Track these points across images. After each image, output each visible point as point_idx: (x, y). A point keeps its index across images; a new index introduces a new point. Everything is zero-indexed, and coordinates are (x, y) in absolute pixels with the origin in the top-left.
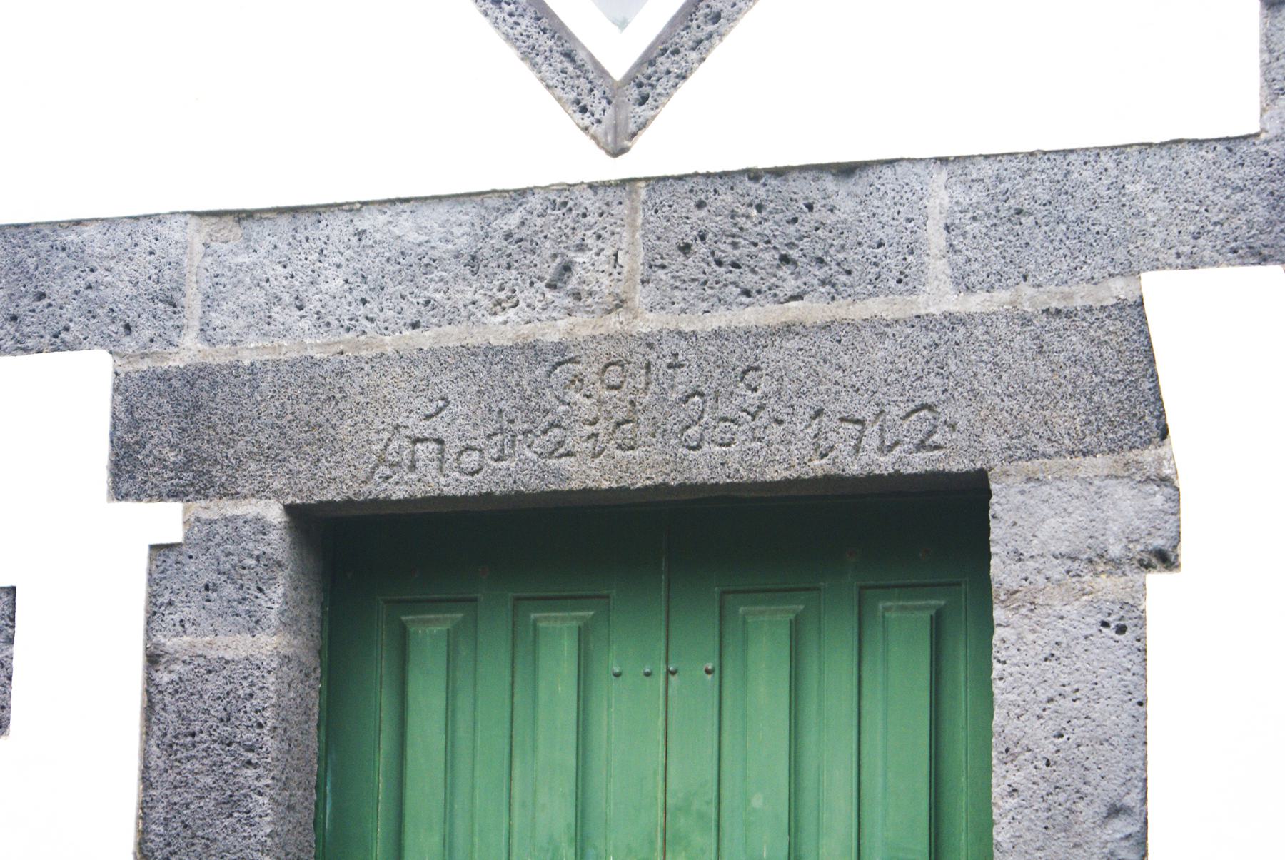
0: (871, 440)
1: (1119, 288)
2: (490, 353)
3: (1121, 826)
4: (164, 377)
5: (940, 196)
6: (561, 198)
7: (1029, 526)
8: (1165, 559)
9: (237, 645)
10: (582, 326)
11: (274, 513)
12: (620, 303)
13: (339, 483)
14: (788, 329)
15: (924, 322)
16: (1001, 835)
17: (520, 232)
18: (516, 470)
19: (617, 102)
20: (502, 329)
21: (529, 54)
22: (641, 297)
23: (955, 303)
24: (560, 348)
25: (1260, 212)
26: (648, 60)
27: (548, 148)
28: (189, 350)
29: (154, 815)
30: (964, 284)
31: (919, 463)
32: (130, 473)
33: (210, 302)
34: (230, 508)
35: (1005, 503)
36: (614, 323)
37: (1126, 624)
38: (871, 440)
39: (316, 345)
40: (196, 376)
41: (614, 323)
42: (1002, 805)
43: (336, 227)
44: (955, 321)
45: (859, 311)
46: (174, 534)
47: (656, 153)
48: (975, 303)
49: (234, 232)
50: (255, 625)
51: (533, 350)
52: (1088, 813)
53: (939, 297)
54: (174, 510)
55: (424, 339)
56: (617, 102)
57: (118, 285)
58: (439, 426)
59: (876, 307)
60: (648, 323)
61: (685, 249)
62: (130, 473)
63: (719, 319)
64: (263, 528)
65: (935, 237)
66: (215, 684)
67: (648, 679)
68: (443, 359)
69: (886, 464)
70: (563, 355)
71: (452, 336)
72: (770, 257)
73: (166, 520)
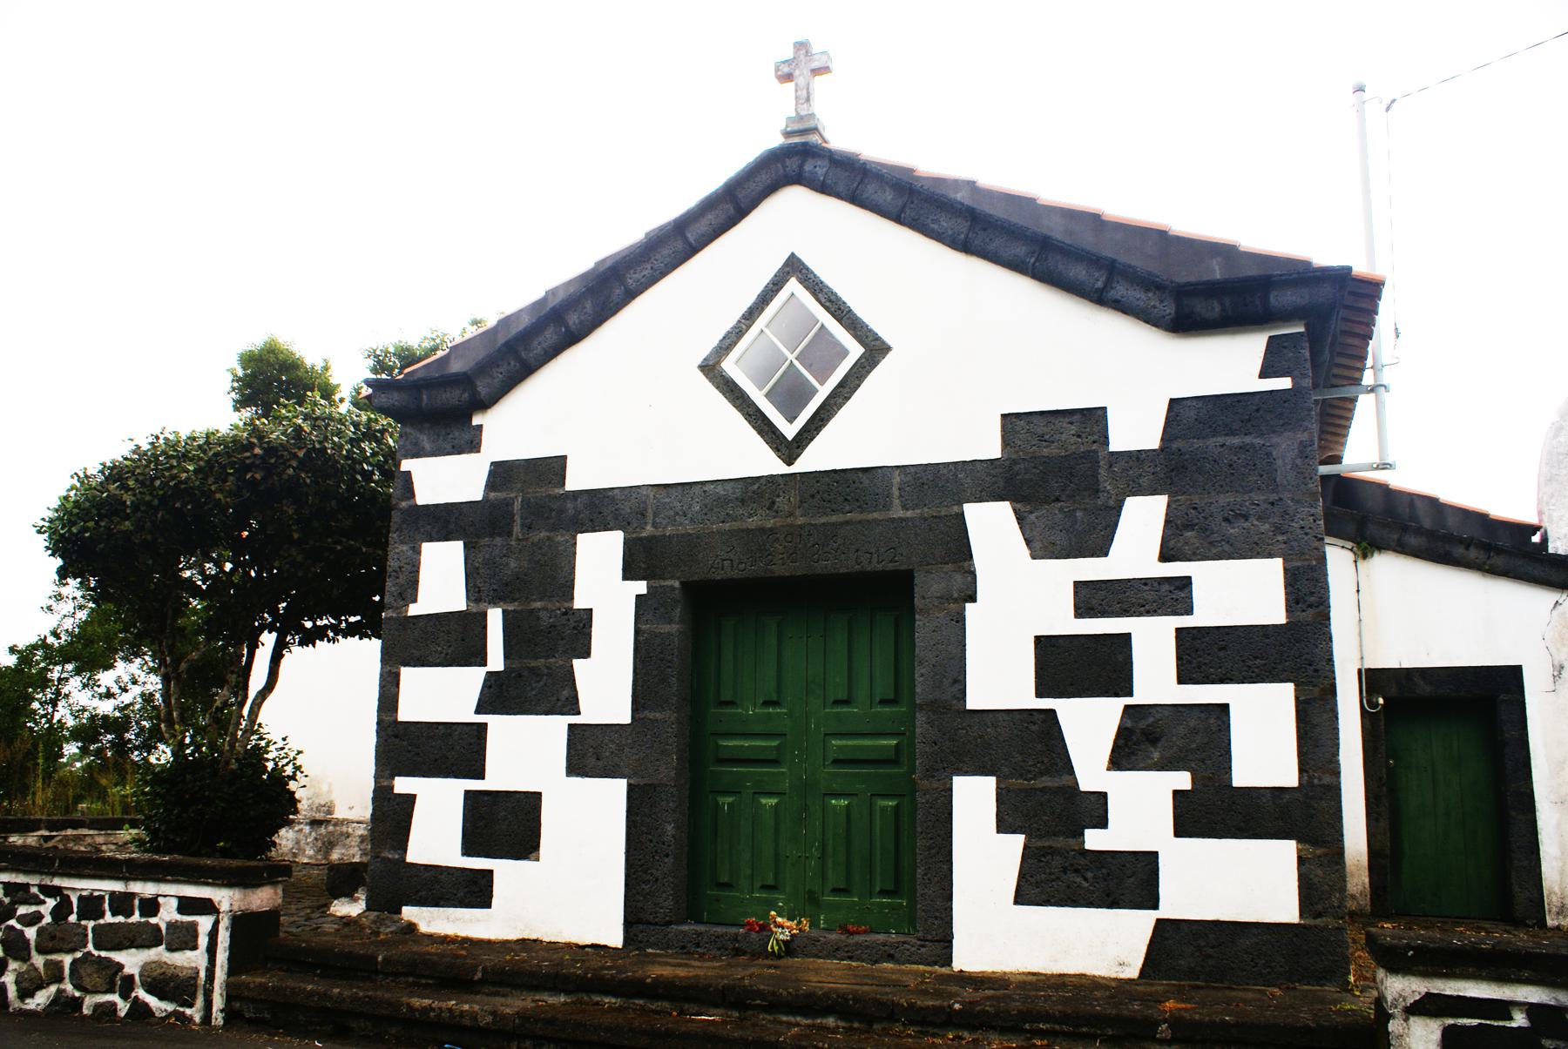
0: (875, 560)
1: (956, 509)
2: (748, 531)
3: (957, 686)
4: (641, 539)
5: (897, 479)
6: (771, 479)
7: (928, 586)
8: (973, 599)
9: (666, 628)
10: (779, 522)
11: (677, 584)
12: (791, 514)
13: (698, 574)
14: (847, 523)
15: (893, 520)
16: (918, 690)
17: (753, 490)
18: (757, 569)
19: (789, 450)
20: (752, 522)
21: (760, 433)
22: (798, 512)
23: (901, 514)
24: (771, 529)
25: (1001, 484)
26: (800, 434)
27: (767, 463)
28: (649, 530)
29: (788, 162)
30: (905, 508)
31: (891, 566)
32: (629, 573)
33: (655, 515)
34: (663, 583)
35: (919, 578)
36: (789, 520)
37: (960, 620)
38: (875, 560)
39: (690, 529)
40: (651, 538)
41: (789, 520)
42: (919, 679)
43: (697, 490)
44: (902, 519)
45: (870, 517)
46: (644, 591)
47: (808, 462)
48: (909, 514)
49: (664, 492)
50: (670, 622)
51: (762, 530)
52: (946, 682)
53: (897, 512)
54: (644, 583)
55: (727, 526)
56: (789, 450)
57: (626, 509)
58: (731, 555)
59: (876, 515)
60: (800, 521)
61: (813, 496)
62: (629, 573)
63: (824, 520)
64: (672, 588)
65: (896, 493)
66: (658, 641)
67: (1123, 958)
68: (731, 532)
69: (880, 567)
70: (772, 531)
71: (736, 525)
72: (840, 499)
73: (641, 587)
